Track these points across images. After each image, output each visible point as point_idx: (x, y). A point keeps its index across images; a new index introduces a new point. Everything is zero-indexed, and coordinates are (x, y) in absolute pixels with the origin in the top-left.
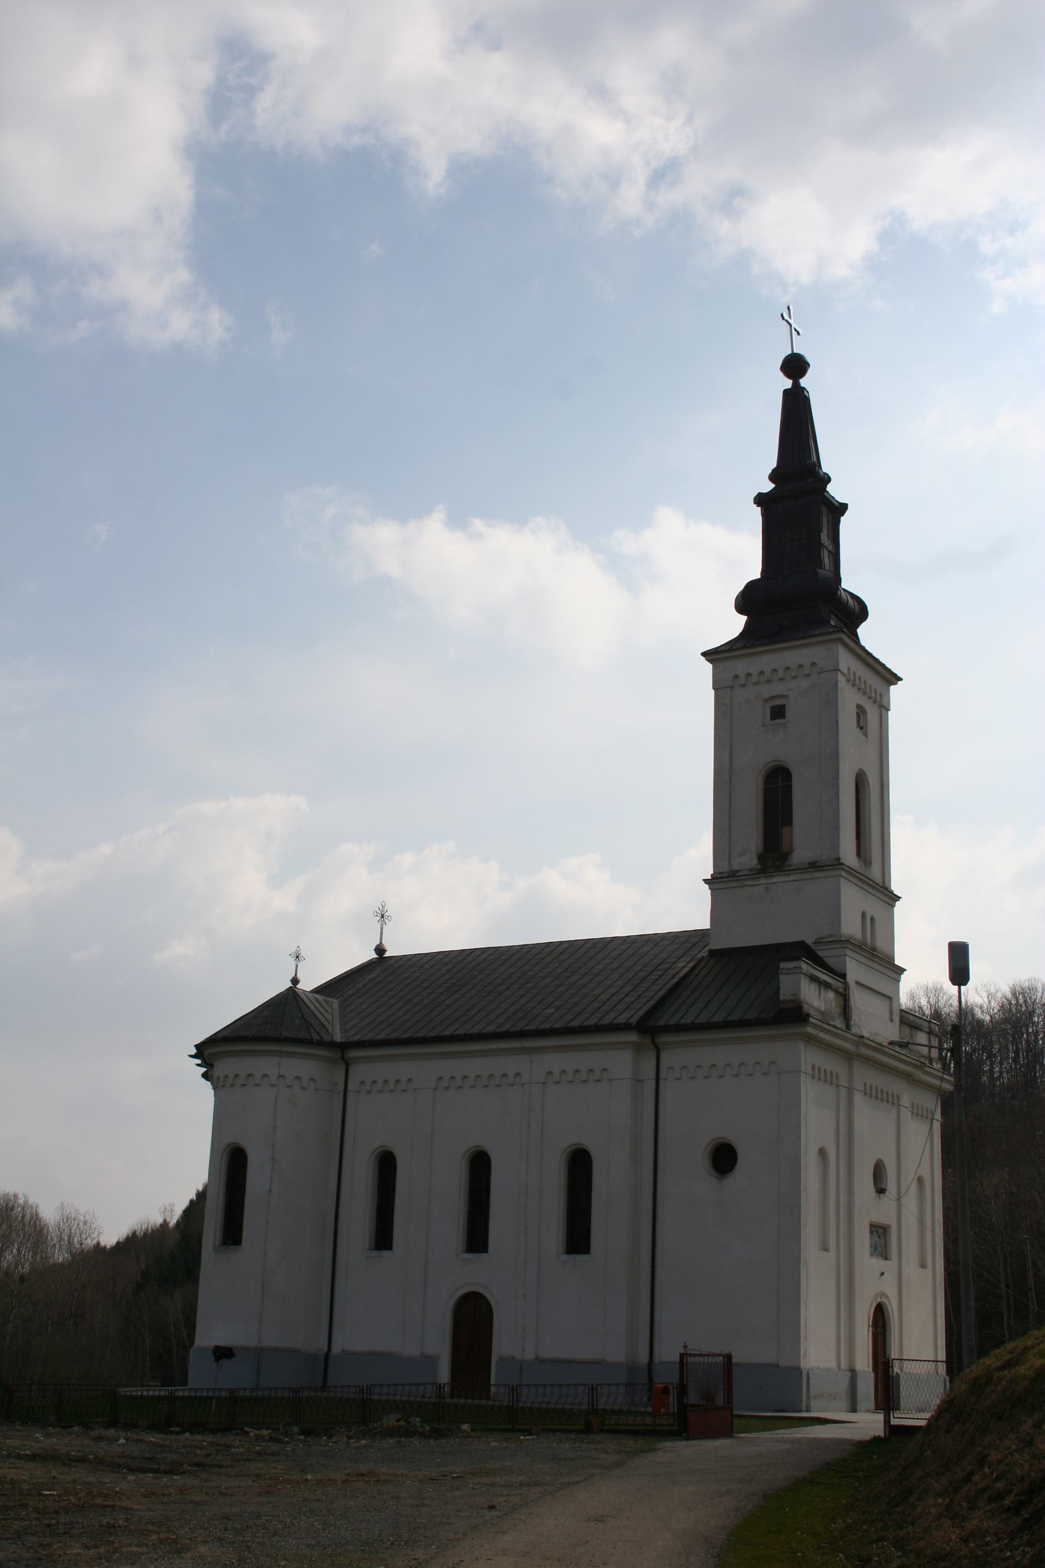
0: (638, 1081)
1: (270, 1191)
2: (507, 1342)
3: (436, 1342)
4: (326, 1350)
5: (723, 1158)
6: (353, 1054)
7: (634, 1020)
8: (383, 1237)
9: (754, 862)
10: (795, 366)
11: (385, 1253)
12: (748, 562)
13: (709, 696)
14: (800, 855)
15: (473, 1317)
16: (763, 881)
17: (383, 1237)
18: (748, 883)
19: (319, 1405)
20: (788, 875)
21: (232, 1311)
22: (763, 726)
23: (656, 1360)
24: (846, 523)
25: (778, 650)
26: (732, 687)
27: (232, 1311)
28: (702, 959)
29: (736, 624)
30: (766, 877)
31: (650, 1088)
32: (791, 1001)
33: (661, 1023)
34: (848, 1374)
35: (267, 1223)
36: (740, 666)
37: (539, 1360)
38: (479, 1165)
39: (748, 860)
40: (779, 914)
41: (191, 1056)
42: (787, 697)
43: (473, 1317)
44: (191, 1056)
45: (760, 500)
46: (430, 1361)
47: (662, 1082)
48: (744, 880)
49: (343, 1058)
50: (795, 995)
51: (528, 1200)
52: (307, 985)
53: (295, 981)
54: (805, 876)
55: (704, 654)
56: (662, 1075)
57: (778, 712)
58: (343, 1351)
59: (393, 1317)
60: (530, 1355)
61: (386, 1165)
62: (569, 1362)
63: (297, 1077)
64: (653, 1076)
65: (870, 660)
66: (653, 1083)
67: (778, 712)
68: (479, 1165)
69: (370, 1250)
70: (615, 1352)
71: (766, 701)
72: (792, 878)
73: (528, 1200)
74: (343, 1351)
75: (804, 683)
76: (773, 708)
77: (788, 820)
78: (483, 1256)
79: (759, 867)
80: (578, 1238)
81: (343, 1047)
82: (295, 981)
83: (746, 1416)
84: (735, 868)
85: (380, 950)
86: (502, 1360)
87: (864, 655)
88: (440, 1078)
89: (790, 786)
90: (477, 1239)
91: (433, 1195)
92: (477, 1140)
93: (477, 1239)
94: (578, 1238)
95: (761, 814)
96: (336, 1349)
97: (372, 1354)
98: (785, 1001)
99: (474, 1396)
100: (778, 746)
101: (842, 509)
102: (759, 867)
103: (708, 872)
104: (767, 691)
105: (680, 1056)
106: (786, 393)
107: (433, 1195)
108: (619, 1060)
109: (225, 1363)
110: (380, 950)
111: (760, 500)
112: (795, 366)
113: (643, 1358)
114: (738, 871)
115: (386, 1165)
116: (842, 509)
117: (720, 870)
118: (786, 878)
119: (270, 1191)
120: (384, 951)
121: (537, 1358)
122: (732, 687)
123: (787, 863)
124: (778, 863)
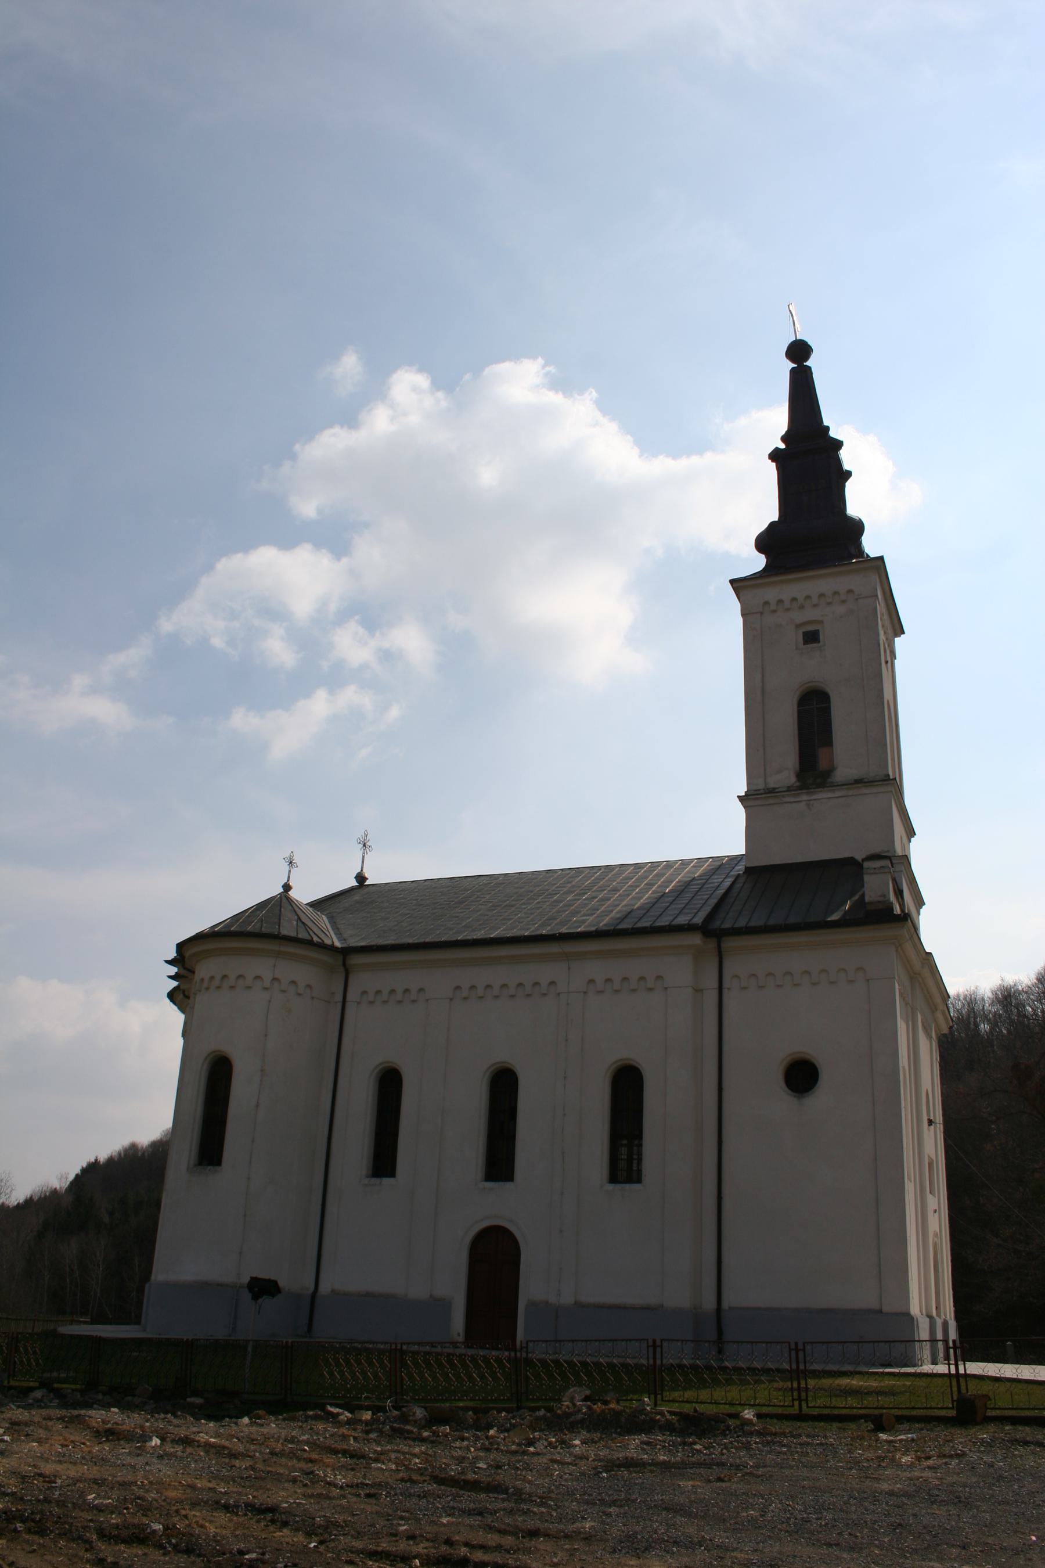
0: (698, 991)
1: (257, 1106)
2: (535, 1285)
3: (450, 1282)
4: (312, 1289)
5: (801, 1076)
6: (356, 960)
7: (699, 920)
8: (384, 1161)
9: (793, 780)
10: (799, 351)
11: (386, 1181)
12: (766, 509)
13: (739, 621)
14: (844, 771)
15: (494, 1256)
16: (805, 797)
17: (384, 1161)
18: (787, 799)
19: (272, 1361)
20: (833, 791)
21: (197, 1249)
22: (797, 648)
23: (725, 1305)
24: (849, 486)
25: (813, 577)
26: (761, 613)
27: (197, 1249)
28: (738, 876)
29: (758, 562)
30: (808, 793)
31: (711, 998)
32: (879, 902)
33: (727, 925)
34: (928, 1320)
35: (253, 1141)
36: (771, 593)
37: (579, 1306)
38: (503, 1085)
39: (787, 776)
40: (822, 832)
41: (167, 962)
42: (821, 622)
43: (494, 1256)
44: (167, 962)
45: (775, 456)
46: (440, 1306)
47: (725, 992)
48: (783, 796)
49: (344, 964)
50: (884, 896)
51: (560, 1121)
52: (304, 894)
53: (287, 887)
54: (851, 792)
55: (732, 582)
56: (726, 984)
57: (812, 637)
58: (333, 1291)
59: (397, 1255)
60: (567, 1298)
61: (389, 1084)
62: (611, 1307)
63: (293, 982)
64: (716, 985)
65: (891, 605)
66: (715, 994)
67: (812, 637)
68: (503, 1085)
69: (367, 1177)
70: (677, 1295)
71: (798, 626)
72: (838, 794)
73: (560, 1121)
74: (333, 1291)
75: (841, 609)
76: (805, 634)
77: (827, 740)
78: (508, 1185)
79: (798, 784)
80: (625, 1162)
81: (346, 952)
82: (287, 887)
83: (877, 1373)
84: (771, 785)
85: (361, 878)
86: (532, 1305)
87: (888, 594)
88: (458, 988)
89: (829, 708)
90: (499, 1164)
91: (444, 1119)
92: (502, 1056)
93: (499, 1164)
94: (625, 1162)
95: (796, 732)
96: (325, 1288)
97: (368, 1294)
98: (871, 903)
99: (492, 1351)
100: (814, 668)
101: (848, 474)
102: (798, 784)
103: (742, 790)
104: (799, 617)
105: (746, 961)
106: (792, 371)
107: (444, 1119)
108: (678, 969)
109: (266, 1301)
110: (361, 878)
111: (775, 456)
112: (799, 351)
113: (709, 1303)
114: (774, 789)
115: (389, 1084)
116: (848, 474)
117: (755, 788)
118: (830, 795)
119: (257, 1106)
120: (366, 879)
121: (576, 1303)
122: (761, 613)
123: (830, 780)
124: (819, 780)
